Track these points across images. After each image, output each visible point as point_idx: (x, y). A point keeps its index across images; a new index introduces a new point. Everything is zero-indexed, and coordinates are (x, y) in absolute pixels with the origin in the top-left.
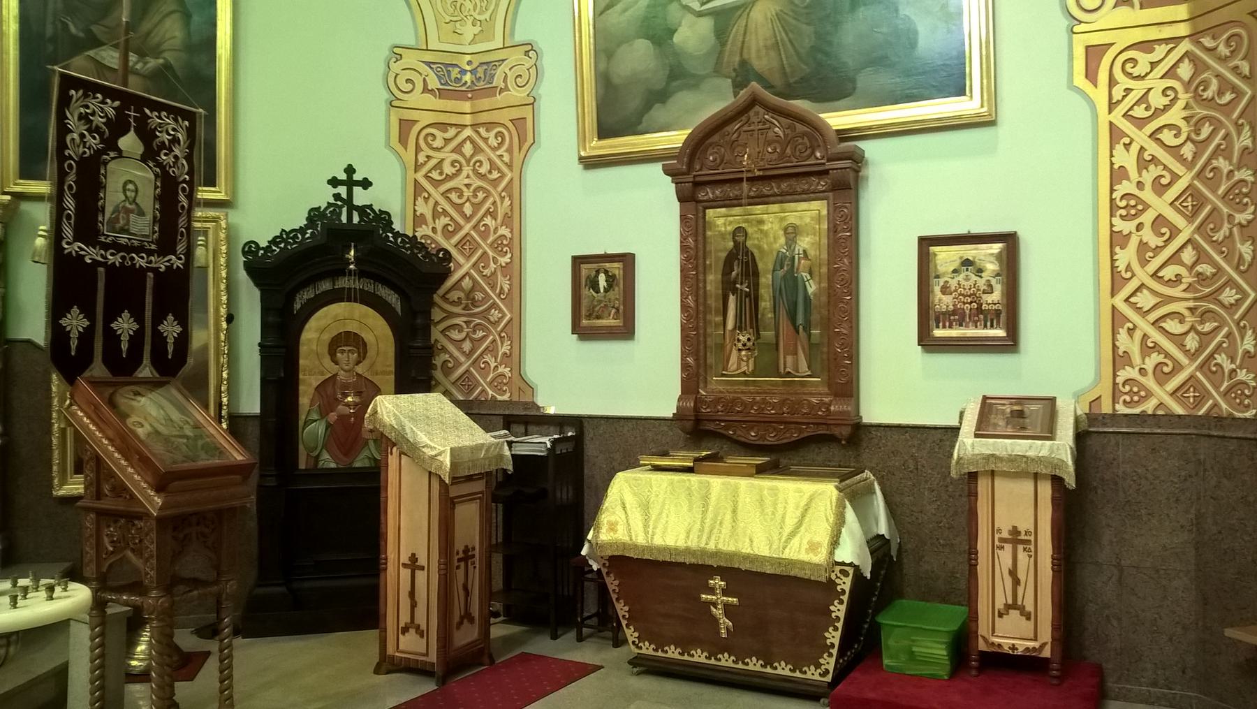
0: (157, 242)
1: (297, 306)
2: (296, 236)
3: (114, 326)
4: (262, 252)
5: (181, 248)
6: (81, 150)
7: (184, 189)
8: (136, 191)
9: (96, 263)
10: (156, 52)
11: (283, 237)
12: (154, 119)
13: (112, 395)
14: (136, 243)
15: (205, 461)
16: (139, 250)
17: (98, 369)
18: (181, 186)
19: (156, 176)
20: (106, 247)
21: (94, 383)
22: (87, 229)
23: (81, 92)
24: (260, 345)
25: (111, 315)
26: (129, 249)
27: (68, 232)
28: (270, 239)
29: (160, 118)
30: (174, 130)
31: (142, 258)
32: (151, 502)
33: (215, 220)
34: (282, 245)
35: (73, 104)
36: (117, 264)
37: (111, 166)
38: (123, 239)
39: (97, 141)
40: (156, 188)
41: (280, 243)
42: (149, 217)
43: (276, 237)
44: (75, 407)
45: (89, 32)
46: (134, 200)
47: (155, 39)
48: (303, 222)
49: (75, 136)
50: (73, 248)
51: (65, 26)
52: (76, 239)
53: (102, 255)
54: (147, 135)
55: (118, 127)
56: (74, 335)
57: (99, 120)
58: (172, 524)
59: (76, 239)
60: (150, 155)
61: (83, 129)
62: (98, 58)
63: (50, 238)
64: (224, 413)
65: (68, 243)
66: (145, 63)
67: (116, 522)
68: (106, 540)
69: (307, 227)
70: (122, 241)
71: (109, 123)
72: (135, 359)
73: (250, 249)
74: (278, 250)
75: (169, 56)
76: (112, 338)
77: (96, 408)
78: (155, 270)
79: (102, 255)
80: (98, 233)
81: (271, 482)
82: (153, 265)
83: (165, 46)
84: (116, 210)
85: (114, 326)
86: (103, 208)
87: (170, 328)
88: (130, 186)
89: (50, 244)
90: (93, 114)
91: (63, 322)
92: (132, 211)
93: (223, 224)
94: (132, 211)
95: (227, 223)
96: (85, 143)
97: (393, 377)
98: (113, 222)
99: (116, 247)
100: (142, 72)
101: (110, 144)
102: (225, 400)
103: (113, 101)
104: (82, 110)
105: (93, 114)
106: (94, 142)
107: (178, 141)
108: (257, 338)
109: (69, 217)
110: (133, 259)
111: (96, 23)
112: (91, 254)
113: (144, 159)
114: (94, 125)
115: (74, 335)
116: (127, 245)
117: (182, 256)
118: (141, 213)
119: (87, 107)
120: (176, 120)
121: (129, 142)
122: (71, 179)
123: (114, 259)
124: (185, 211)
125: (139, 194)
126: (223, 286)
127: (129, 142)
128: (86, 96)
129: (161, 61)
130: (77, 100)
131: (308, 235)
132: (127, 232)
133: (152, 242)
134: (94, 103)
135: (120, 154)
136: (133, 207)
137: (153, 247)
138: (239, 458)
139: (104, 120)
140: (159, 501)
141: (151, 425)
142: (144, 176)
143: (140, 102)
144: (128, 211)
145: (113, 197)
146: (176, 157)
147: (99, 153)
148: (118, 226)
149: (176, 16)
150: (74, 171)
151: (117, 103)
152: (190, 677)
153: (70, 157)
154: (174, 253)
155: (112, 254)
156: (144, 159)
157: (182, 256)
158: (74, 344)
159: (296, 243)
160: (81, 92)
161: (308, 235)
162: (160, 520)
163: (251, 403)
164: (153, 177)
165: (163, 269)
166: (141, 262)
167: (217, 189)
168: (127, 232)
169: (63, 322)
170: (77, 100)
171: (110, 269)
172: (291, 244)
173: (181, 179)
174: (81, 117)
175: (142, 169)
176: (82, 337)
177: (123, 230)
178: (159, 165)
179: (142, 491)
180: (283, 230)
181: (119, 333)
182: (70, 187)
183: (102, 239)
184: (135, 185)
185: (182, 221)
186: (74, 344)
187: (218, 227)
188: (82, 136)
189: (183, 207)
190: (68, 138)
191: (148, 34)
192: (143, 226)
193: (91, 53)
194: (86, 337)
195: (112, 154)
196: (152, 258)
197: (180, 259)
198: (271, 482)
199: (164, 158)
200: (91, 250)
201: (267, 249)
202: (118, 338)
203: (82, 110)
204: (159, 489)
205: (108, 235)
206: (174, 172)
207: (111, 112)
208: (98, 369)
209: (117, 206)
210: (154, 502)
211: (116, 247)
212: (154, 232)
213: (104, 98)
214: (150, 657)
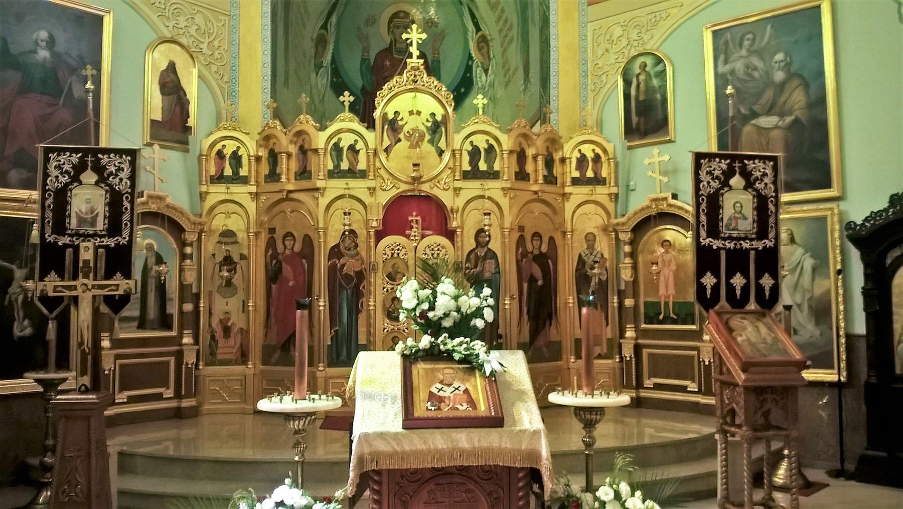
0: (757, 233)
1: (889, 261)
2: (882, 215)
3: (732, 281)
4: (858, 228)
5: (772, 235)
6: (708, 190)
7: (772, 201)
8: (742, 206)
9: (719, 249)
10: (790, 113)
11: (874, 215)
12: (750, 165)
13: (728, 319)
14: (743, 236)
15: (774, 357)
16: (744, 239)
17: (752, 306)
18: (770, 200)
19: (754, 196)
20: (725, 239)
21: (719, 314)
22: (714, 232)
23: (707, 160)
24: (863, 288)
25: (730, 276)
26: (738, 239)
27: (703, 233)
28: (863, 219)
29: (754, 163)
30: (764, 168)
31: (747, 243)
32: (739, 377)
33: (831, 209)
34: (872, 222)
35: (703, 167)
36: (732, 248)
37: (726, 195)
38: (735, 234)
39: (718, 183)
40: (754, 203)
41: (871, 220)
42: (750, 220)
43: (868, 217)
44: (710, 325)
45: (752, 110)
46: (740, 212)
47: (788, 106)
48: (886, 205)
49: (705, 183)
50: (706, 241)
51: (739, 110)
52: (708, 236)
53: (723, 244)
54: (746, 174)
55: (729, 174)
56: (709, 287)
57: (717, 173)
58: (756, 392)
59: (708, 236)
60: (749, 185)
61: (709, 178)
62: (757, 124)
63: (693, 238)
64: (842, 333)
65: (703, 239)
66: (784, 121)
67: (729, 387)
68: (725, 397)
69: (889, 207)
70: (735, 235)
71: (724, 173)
72: (745, 299)
73: (849, 226)
74: (869, 225)
75: (798, 113)
76: (731, 288)
77: (717, 326)
78: (756, 249)
79: (723, 244)
80: (719, 232)
81: (874, 380)
82: (754, 246)
83: (796, 107)
84: (730, 219)
85: (732, 281)
86: (722, 219)
87: (767, 281)
88: (738, 205)
89: (693, 241)
90: (714, 170)
91: (703, 280)
92: (740, 218)
93: (836, 211)
94: (740, 218)
95: (839, 211)
96: (710, 186)
97: (139, 301)
98: (728, 226)
99: (731, 238)
100: (782, 126)
101: (725, 184)
102: (842, 325)
103: (726, 160)
104: (708, 169)
105: (714, 170)
106: (715, 184)
107: (767, 174)
108: (862, 284)
109: (703, 226)
110: (741, 244)
111: (754, 104)
112: (716, 244)
113: (746, 188)
114: (715, 175)
115: (709, 287)
116: (737, 237)
117: (773, 240)
118: (745, 218)
119: (711, 167)
120: (765, 163)
121: (737, 181)
122: (704, 206)
123: (730, 245)
124: (773, 214)
125: (743, 208)
126: (838, 251)
127: (737, 181)
128: (709, 161)
129: (793, 117)
130: (705, 165)
131: (890, 213)
132: (737, 230)
133: (752, 234)
134: (715, 164)
135: (731, 188)
136: (740, 216)
137: (754, 236)
138: (798, 357)
139: (721, 172)
140: (743, 376)
141: (746, 336)
142: (747, 200)
143: (742, 158)
144: (736, 219)
145: (727, 212)
146: (766, 184)
147: (718, 190)
148: (731, 227)
149: (800, 88)
150: (705, 201)
151: (728, 161)
152: (807, 495)
153: (702, 195)
154: (767, 238)
155: (729, 243)
156: (746, 188)
157: (773, 240)
158: (709, 292)
159: (881, 219)
160: (707, 160)
161: (890, 213)
162: (746, 388)
163: (860, 327)
164: (751, 197)
165: (761, 248)
166: (746, 245)
167: (832, 190)
168: (737, 230)
169: (703, 280)
170: (705, 165)
171: (728, 251)
172: (878, 220)
173: (770, 196)
174: (707, 173)
175: (744, 194)
176: (713, 288)
177: (734, 229)
178: (756, 190)
179: (736, 371)
180: (872, 212)
181: (735, 285)
182: (703, 210)
183: (723, 235)
184: (740, 203)
185: (771, 220)
186: (709, 292)
187: (833, 215)
188: (709, 182)
189: (772, 212)
190: (701, 185)
191: (785, 102)
192: (747, 225)
193: (753, 122)
194: (716, 288)
195: (726, 189)
196: (753, 243)
197: (771, 241)
198: (874, 380)
199: (758, 185)
200: (716, 242)
201: (863, 224)
202: (734, 289)
203: (708, 169)
204: (744, 370)
205: (725, 233)
206: (765, 193)
207: (724, 167)
208: (752, 306)
209: (731, 217)
210: (741, 377)
211: (731, 238)
212: (753, 228)
213: (720, 160)
214: (786, 477)
